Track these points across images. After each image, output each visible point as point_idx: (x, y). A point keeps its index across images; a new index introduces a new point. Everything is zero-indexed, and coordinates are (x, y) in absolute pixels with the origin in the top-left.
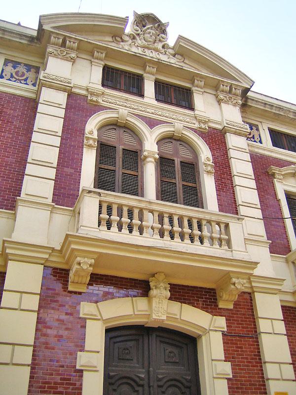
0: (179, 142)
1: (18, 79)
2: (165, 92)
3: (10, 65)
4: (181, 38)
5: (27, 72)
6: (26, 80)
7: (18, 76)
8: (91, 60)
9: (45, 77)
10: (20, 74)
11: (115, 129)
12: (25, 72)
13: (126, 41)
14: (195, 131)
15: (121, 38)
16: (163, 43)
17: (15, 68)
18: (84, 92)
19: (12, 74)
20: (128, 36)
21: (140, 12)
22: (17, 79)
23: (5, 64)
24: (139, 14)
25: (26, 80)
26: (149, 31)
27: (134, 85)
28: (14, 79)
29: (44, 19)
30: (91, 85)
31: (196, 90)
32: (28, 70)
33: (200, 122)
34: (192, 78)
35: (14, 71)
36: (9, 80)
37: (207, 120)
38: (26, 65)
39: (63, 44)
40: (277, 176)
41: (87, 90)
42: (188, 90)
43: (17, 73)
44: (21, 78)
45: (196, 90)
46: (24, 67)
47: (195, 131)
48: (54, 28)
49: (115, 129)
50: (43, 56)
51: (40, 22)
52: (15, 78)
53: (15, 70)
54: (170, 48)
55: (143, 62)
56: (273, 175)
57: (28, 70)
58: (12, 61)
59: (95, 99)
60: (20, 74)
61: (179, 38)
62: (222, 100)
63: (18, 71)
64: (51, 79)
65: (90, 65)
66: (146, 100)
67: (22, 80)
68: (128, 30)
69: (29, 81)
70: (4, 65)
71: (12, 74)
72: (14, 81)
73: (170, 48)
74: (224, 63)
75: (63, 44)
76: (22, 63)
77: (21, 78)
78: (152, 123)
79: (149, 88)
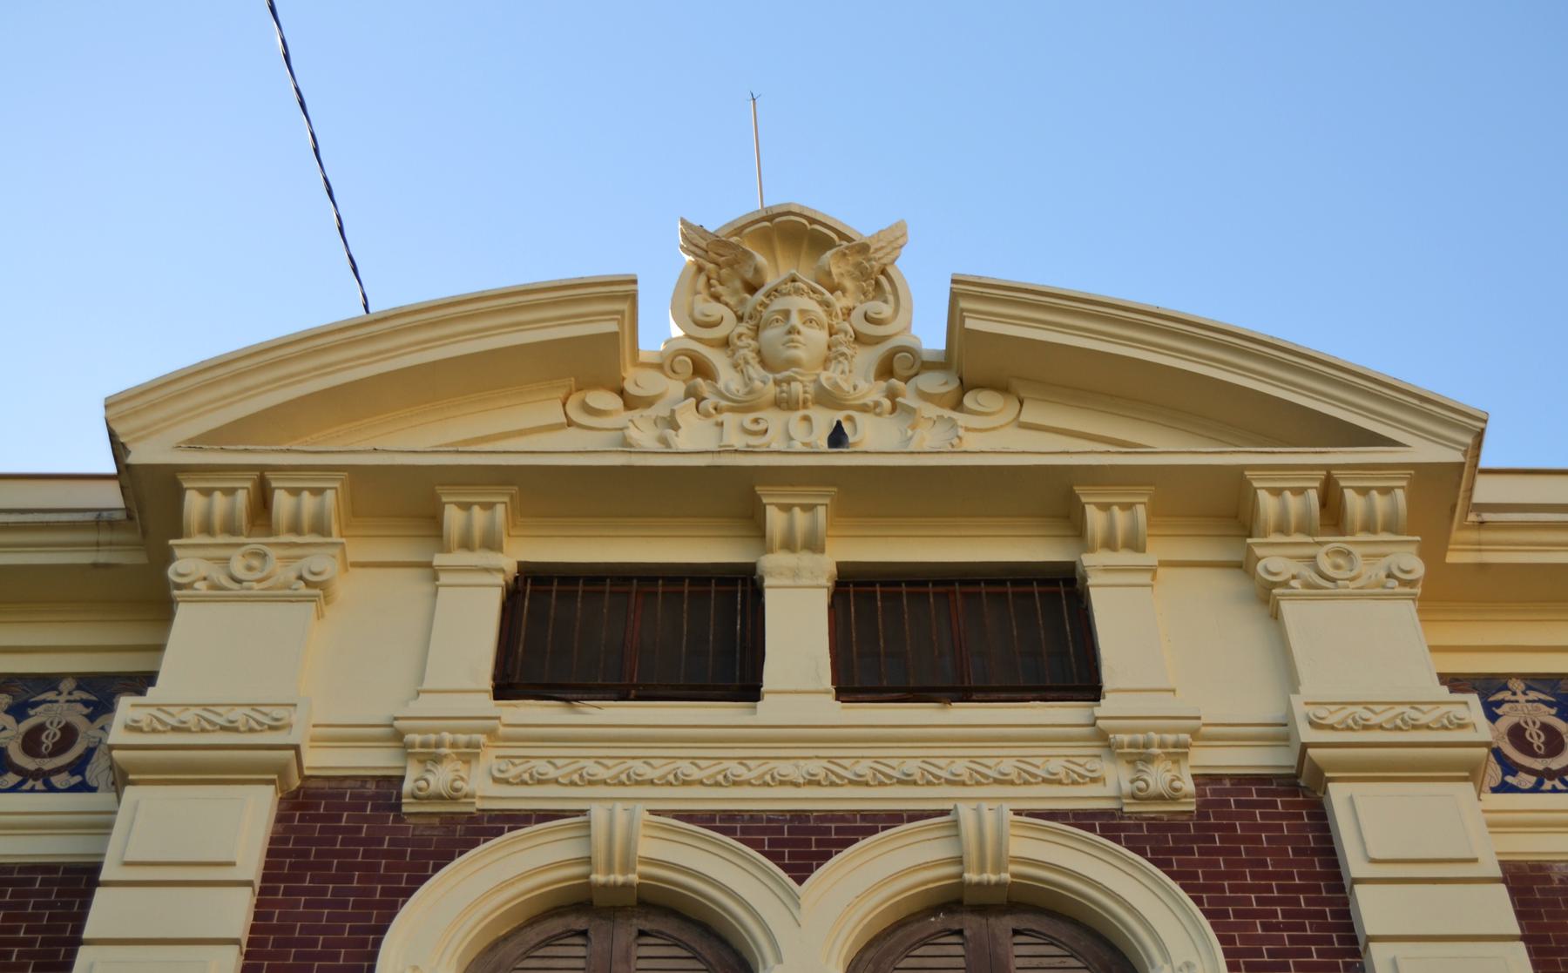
0: (1009, 922)
1: (38, 774)
2: (909, 636)
4: (964, 292)
5: (91, 718)
6: (79, 766)
7: (1534, 755)
8: (429, 565)
9: (133, 728)
11: (584, 933)
13: (648, 402)
14: (1105, 824)
15: (621, 392)
16: (881, 350)
18: (375, 760)
19: (1497, 753)
20: (659, 367)
21: (715, 221)
22: (25, 775)
24: (711, 229)
26: (779, 304)
27: (695, 637)
30: (427, 705)
31: (1107, 569)
33: (1140, 756)
34: (1055, 496)
36: (1504, 788)
37: (1185, 737)
39: (1332, 513)
41: (399, 736)
42: (1054, 582)
44: (49, 764)
45: (1107, 569)
47: (1105, 824)
48: (193, 444)
49: (584, 933)
50: (154, 602)
51: (112, 436)
52: (19, 770)
54: (928, 366)
55: (734, 494)
59: (440, 778)
61: (954, 297)
62: (1285, 584)
63: (40, 728)
64: (223, 728)
65: (427, 588)
66: (768, 710)
67: (58, 771)
68: (660, 329)
72: (1536, 789)
73: (928, 366)
75: (1332, 513)
76: (60, 677)
77: (49, 764)
78: (802, 845)
79: (797, 631)
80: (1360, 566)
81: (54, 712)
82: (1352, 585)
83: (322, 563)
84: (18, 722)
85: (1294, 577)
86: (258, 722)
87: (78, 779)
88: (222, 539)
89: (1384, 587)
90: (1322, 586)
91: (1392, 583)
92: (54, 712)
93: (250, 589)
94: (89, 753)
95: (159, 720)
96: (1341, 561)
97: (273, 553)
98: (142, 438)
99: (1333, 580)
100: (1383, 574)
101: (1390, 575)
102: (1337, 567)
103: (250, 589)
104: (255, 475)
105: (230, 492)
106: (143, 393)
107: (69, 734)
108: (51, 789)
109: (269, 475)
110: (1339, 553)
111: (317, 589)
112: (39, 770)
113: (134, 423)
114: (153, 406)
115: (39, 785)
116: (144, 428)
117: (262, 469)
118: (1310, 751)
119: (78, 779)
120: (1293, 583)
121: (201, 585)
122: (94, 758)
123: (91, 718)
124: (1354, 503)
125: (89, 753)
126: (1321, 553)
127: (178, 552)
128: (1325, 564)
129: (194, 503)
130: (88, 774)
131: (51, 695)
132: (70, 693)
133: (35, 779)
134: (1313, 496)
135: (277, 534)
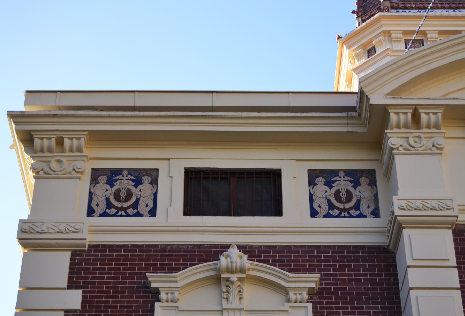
3: (320, 180)
5: (136, 186)
6: (357, 206)
10: (343, 196)
12: (133, 189)
17: (112, 186)
23: (94, 181)
25: (357, 206)
28: (336, 212)
29: (370, 84)
32: (356, 184)
35: (331, 193)
36: (328, 215)
38: (348, 173)
40: (163, 296)
43: (117, 196)
46: (347, 178)
53: (334, 190)
56: (155, 294)
57: (356, 184)
58: (320, 173)
60: (343, 196)
62: (397, 149)
63: (118, 191)
69: (364, 208)
70: (310, 184)
71: (108, 200)
74: (392, 78)
76: (339, 171)
80: (424, 141)
81: (124, 184)
82: (420, 149)
83: (439, 140)
84: (111, 187)
85: (401, 146)
86: (442, 207)
87: (136, 211)
88: (403, 130)
89: (431, 150)
90: (410, 150)
91: (434, 149)
92: (124, 184)
93: (418, 150)
94: (138, 200)
95: (409, 205)
96: (417, 140)
97: (422, 135)
98: (372, 93)
99: (414, 147)
100: (431, 145)
101: (434, 146)
102: (415, 142)
103: (418, 150)
104: (413, 107)
105: (405, 113)
106: (367, 79)
107: (129, 195)
108: (128, 215)
109: (418, 107)
110: (417, 137)
111: (438, 150)
112: (122, 207)
113: (370, 88)
114: (375, 81)
115: (124, 213)
116: (373, 89)
117: (416, 105)
118: (398, 218)
119: (136, 211)
120: (401, 148)
121: (401, 148)
122: (140, 203)
123: (136, 186)
124: (424, 118)
125: (138, 200)
126: (411, 136)
127: (389, 135)
128: (411, 141)
129: (393, 117)
130: (139, 209)
131: (120, 177)
132: (127, 176)
133: (122, 211)
134: (410, 115)
135: (422, 129)
